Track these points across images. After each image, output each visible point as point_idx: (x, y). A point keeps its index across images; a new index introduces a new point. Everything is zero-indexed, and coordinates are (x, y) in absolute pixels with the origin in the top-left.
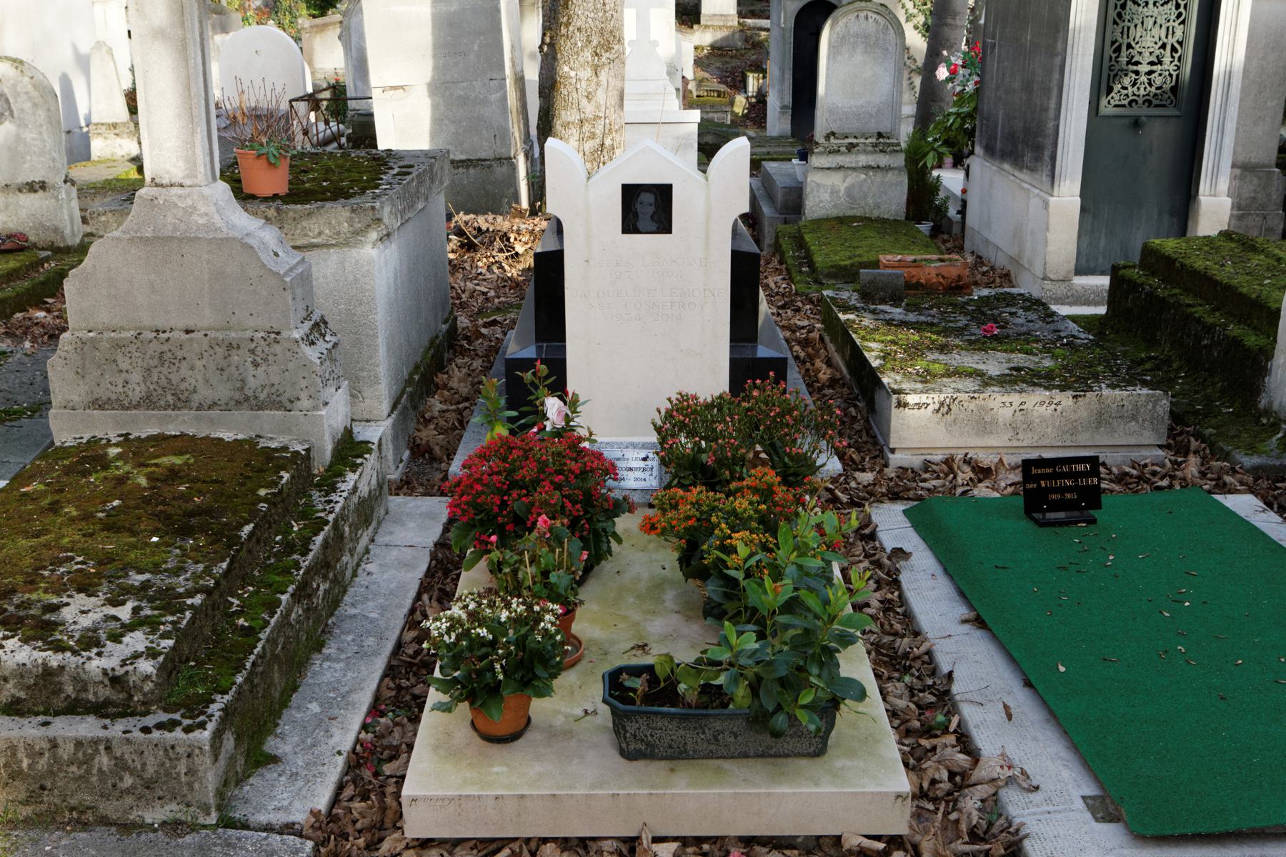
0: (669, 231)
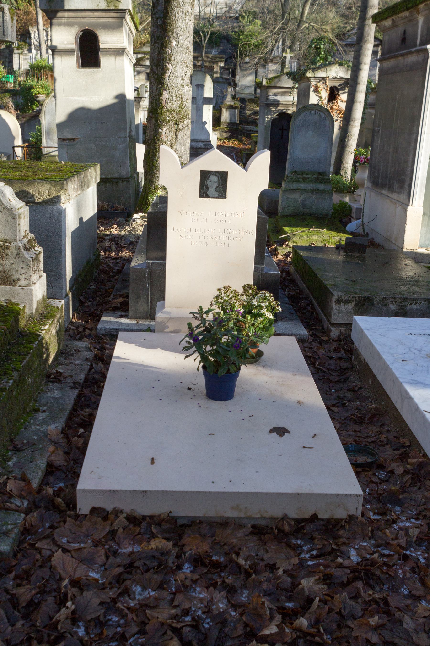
0: (225, 198)
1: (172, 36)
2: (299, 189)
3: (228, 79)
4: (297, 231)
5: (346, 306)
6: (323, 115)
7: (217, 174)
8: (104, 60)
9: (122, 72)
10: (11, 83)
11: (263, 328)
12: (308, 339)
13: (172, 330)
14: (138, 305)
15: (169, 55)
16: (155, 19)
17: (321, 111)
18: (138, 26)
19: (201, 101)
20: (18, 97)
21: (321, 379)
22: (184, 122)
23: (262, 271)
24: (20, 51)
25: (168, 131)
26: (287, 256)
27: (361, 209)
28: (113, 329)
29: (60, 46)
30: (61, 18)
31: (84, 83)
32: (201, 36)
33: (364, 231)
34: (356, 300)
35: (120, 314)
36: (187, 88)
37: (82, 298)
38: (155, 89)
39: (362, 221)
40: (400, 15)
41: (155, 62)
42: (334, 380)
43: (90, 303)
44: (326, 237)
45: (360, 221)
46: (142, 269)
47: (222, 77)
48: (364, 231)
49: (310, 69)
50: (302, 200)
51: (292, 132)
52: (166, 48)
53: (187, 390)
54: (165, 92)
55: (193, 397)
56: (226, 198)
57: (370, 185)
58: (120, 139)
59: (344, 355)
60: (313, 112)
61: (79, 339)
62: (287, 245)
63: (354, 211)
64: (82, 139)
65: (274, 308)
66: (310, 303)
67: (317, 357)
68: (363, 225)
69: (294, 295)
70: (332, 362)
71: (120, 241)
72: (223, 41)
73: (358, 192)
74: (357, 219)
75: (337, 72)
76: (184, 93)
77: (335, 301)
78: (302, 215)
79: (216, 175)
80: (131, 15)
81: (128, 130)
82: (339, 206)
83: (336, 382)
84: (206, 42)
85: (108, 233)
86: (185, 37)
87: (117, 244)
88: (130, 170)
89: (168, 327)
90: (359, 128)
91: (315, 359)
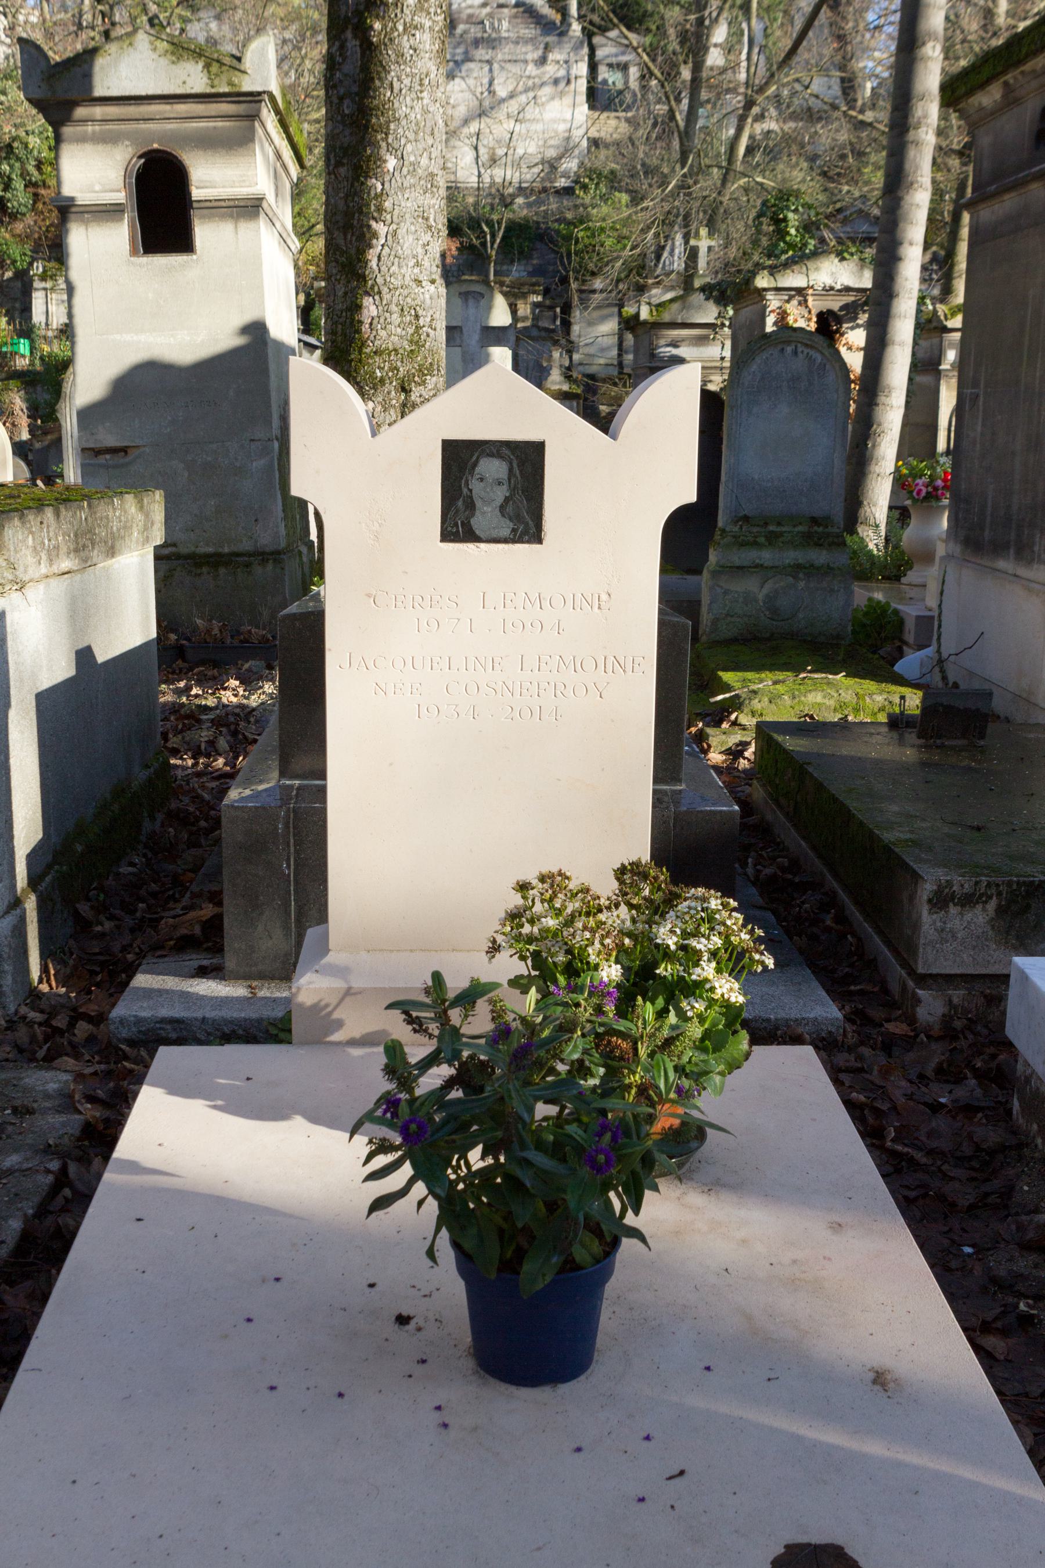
1: (384, 145)
2: (756, 566)
3: (553, 331)
4: (761, 681)
5: (968, 916)
6: (819, 358)
7: (505, 451)
8: (203, 232)
9: (254, 263)
10: (23, 356)
11: (702, 1040)
12: (845, 1034)
13: (357, 1034)
14: (250, 934)
15: (377, 196)
16: (335, 100)
17: (812, 347)
18: (304, 152)
19: (476, 337)
20: (39, 388)
21: (916, 1199)
22: (424, 382)
23: (677, 803)
24: (49, 284)
25: (379, 408)
26: (736, 753)
27: (933, 617)
28: (163, 1020)
29: (83, 198)
30: (84, 121)
31: (150, 295)
32: (484, 232)
33: (944, 678)
34: (999, 894)
35: (195, 964)
36: (432, 288)
37: (84, 908)
38: (340, 293)
39: (939, 651)
40: (1027, 67)
41: (338, 218)
42: (964, 1202)
43: (108, 925)
44: (848, 696)
45: (930, 651)
46: (263, 808)
47: (538, 327)
48: (944, 678)
49: (764, 268)
50: (767, 596)
51: (732, 408)
52: (367, 177)
53: (391, 1329)
54: (367, 301)
55: (419, 1370)
56: (540, 541)
57: (957, 549)
58: (253, 446)
59: (978, 1092)
60: (789, 349)
61: (44, 1059)
62: (735, 723)
63: (910, 625)
64: (147, 450)
65: (741, 955)
66: (830, 902)
67: (885, 1107)
68: (941, 662)
69: (775, 875)
70: (940, 1122)
71: (242, 724)
72: (538, 245)
73: (912, 576)
74: (920, 647)
75: (838, 274)
76: (423, 302)
77: (930, 901)
78: (768, 639)
79: (499, 456)
80: (277, 112)
81: (276, 423)
82: (866, 614)
83: (971, 1207)
84: (496, 246)
85: (211, 702)
86: (421, 146)
87: (235, 733)
88: (283, 531)
89: (339, 1024)
90: (902, 411)
91: (878, 1112)
